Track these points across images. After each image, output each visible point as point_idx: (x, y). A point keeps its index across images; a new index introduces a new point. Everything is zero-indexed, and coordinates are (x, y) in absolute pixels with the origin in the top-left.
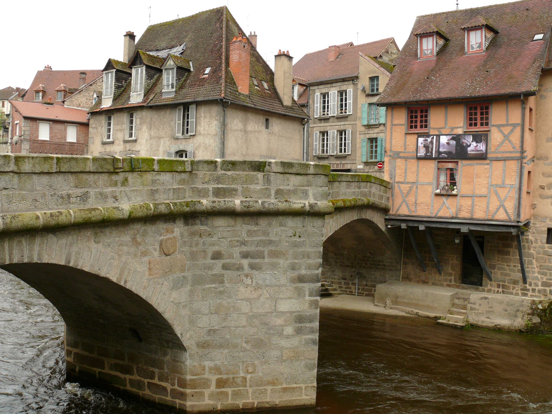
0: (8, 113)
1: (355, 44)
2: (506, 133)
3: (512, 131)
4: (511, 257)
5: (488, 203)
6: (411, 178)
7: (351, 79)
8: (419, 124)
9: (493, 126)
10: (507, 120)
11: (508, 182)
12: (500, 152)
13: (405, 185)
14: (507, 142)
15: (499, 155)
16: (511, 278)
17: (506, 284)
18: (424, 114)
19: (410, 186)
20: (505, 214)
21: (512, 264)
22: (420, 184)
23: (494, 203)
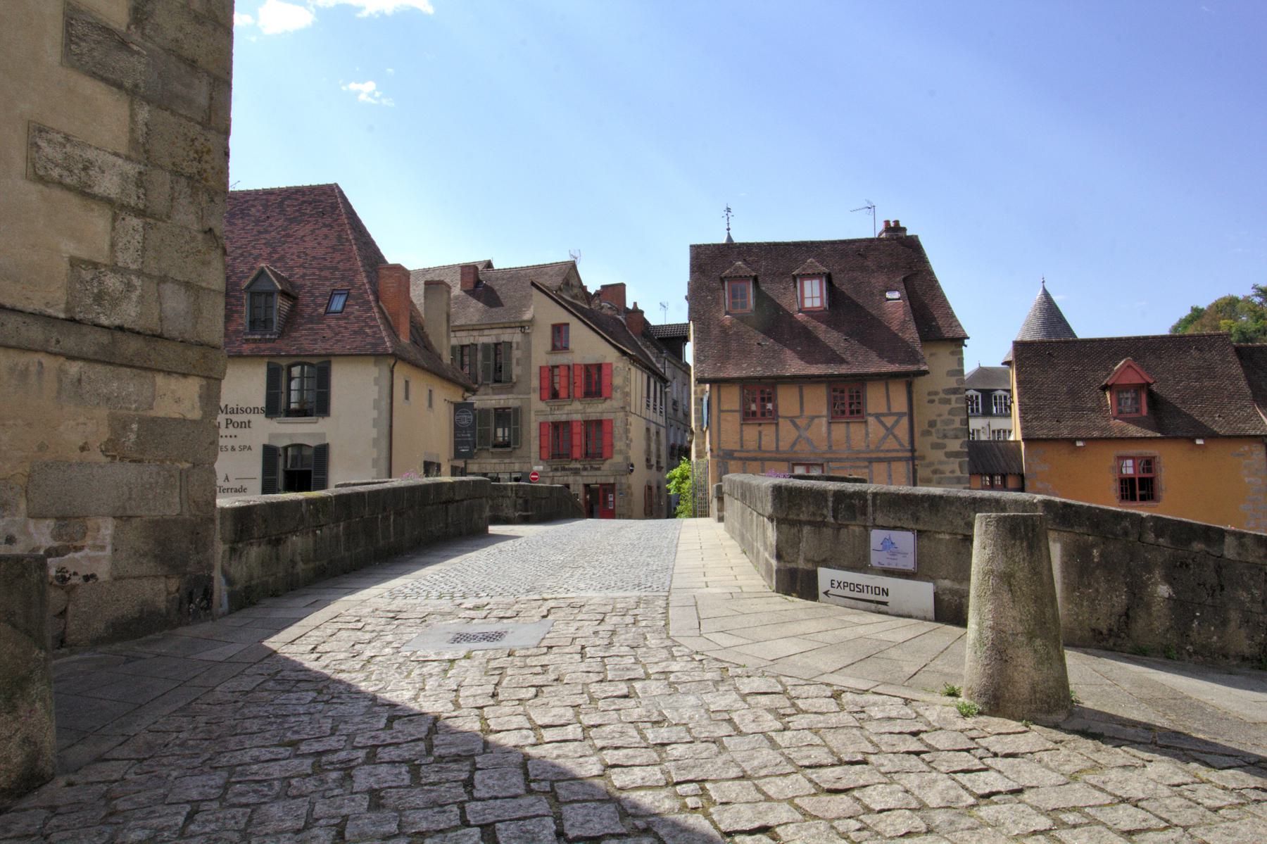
3: (897, 422)
9: (869, 414)
10: (889, 408)
12: (882, 451)
14: (891, 436)
15: (882, 455)
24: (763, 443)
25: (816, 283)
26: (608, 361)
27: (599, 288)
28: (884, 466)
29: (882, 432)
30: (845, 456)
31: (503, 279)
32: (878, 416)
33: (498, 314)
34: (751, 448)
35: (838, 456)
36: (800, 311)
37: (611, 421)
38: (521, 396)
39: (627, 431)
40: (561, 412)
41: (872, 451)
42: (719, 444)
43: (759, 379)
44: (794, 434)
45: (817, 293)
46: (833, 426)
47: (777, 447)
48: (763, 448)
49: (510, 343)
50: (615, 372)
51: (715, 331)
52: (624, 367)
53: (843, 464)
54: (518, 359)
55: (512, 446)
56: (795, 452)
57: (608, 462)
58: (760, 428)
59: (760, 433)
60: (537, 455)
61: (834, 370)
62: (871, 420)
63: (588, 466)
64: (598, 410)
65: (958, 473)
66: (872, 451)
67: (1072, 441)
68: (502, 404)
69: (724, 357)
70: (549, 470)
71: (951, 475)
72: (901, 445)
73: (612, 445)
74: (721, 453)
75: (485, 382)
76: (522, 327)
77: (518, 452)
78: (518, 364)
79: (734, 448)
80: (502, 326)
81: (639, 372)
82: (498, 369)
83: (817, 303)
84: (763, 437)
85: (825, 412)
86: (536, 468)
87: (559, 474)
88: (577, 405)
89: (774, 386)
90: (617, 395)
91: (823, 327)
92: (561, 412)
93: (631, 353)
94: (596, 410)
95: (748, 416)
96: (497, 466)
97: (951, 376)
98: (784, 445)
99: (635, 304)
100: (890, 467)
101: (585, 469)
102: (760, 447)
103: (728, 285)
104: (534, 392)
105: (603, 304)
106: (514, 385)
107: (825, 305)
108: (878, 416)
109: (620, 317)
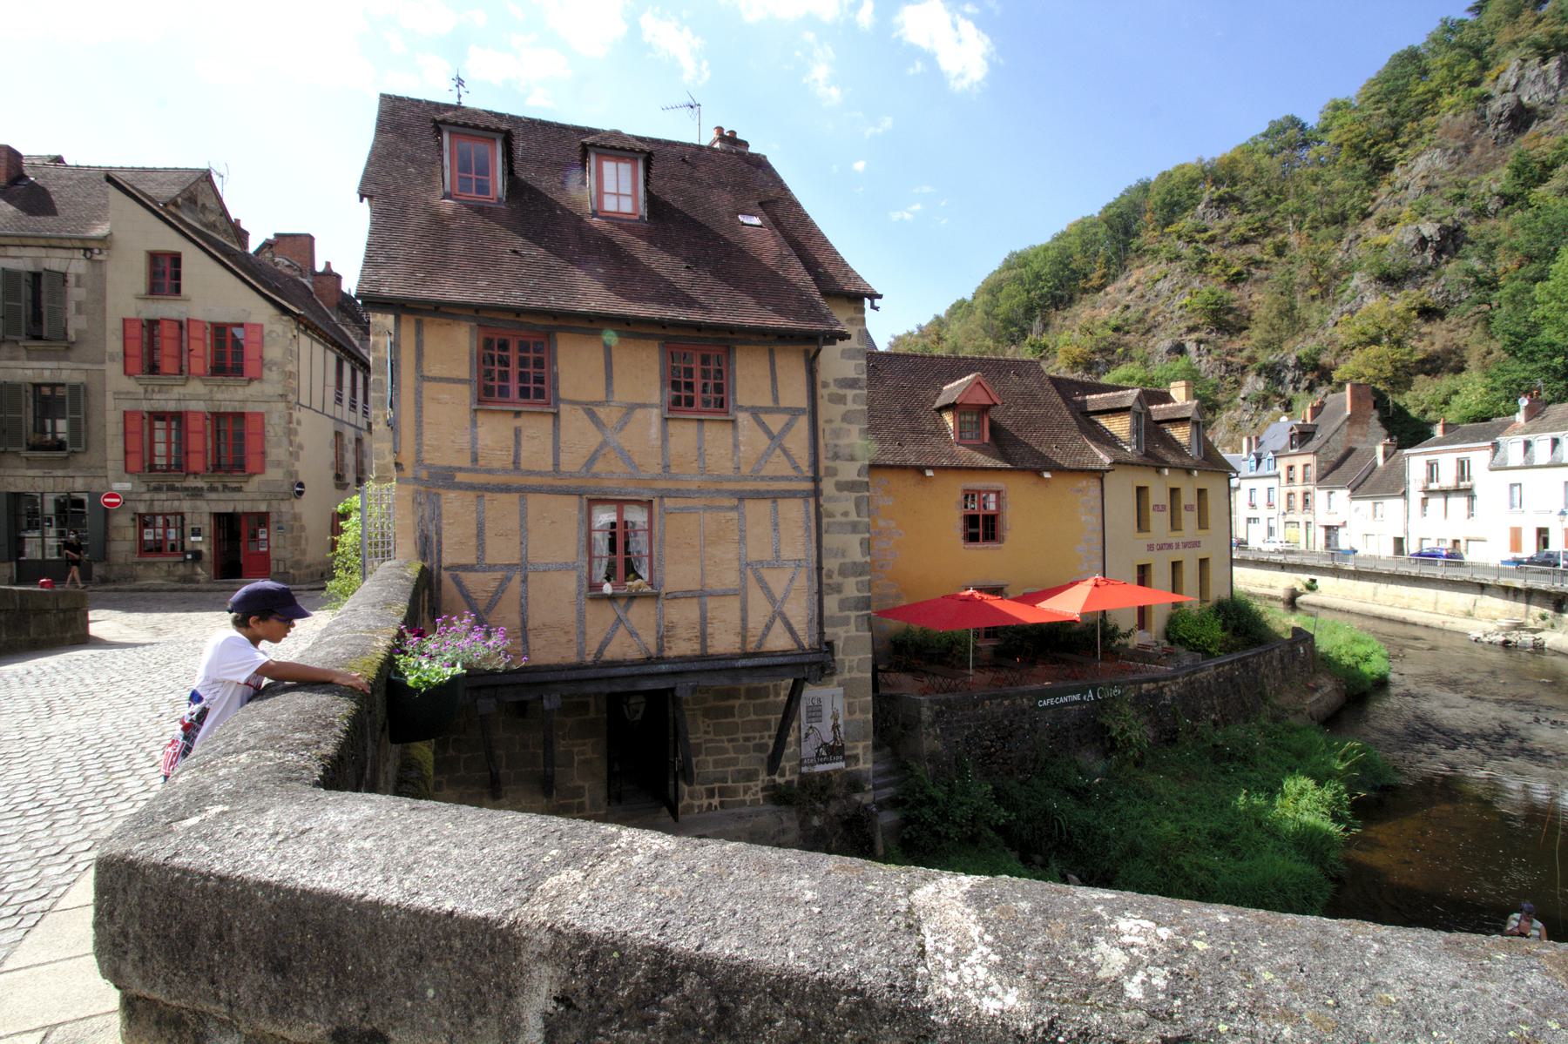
0: (1468, 558)
1: (69, 161)
2: (776, 429)
3: (788, 427)
4: (736, 719)
5: (744, 610)
6: (501, 551)
7: (79, 244)
8: (514, 386)
9: (741, 408)
10: (776, 399)
11: (787, 553)
12: (763, 478)
13: (481, 575)
14: (778, 451)
15: (762, 486)
16: (740, 767)
17: (730, 784)
18: (532, 355)
19: (499, 575)
20: (788, 634)
21: (740, 735)
22: (536, 571)
23: (759, 612)
24: (524, 454)
25: (625, 168)
26: (254, 320)
27: (271, 237)
28: (766, 506)
29: (763, 442)
30: (694, 487)
31: (71, 179)
32: (755, 412)
33: (44, 225)
34: (496, 465)
35: (680, 486)
36: (595, 214)
37: (261, 415)
38: (86, 366)
39: (290, 433)
40: (167, 396)
41: (745, 478)
42: (419, 452)
43: (518, 311)
44: (594, 438)
45: (626, 188)
46: (674, 428)
47: (556, 464)
48: (524, 465)
49: (64, 275)
50: (267, 339)
51: (417, 220)
52: (284, 333)
53: (690, 503)
54: (79, 305)
55: (69, 449)
56: (595, 476)
57: (256, 479)
58: (519, 422)
59: (517, 432)
60: (121, 465)
61: (682, 315)
62: (744, 419)
63: (220, 486)
64: (237, 397)
65: (853, 517)
66: (745, 478)
67: (920, 470)
68: (47, 376)
69: (435, 262)
70: (144, 489)
71: (844, 519)
72: (796, 468)
73: (263, 453)
74: (424, 474)
75: (8, 337)
76: (86, 249)
77: (81, 458)
78: (79, 311)
79: (456, 464)
80: (42, 242)
81: (318, 349)
82: (37, 317)
83: (626, 206)
84: (524, 442)
85: (656, 397)
86: (117, 487)
87: (163, 496)
88: (196, 387)
89: (549, 335)
90: (272, 375)
91: (643, 244)
92: (167, 396)
93: (297, 311)
94: (231, 396)
95: (488, 393)
96: (39, 482)
97: (849, 358)
98: (572, 461)
99: (328, 264)
100: (776, 511)
101: (212, 489)
102: (516, 462)
103: (451, 143)
104: (113, 359)
105: (277, 259)
106: (71, 346)
107: (643, 211)
108: (755, 412)
109: (305, 281)
